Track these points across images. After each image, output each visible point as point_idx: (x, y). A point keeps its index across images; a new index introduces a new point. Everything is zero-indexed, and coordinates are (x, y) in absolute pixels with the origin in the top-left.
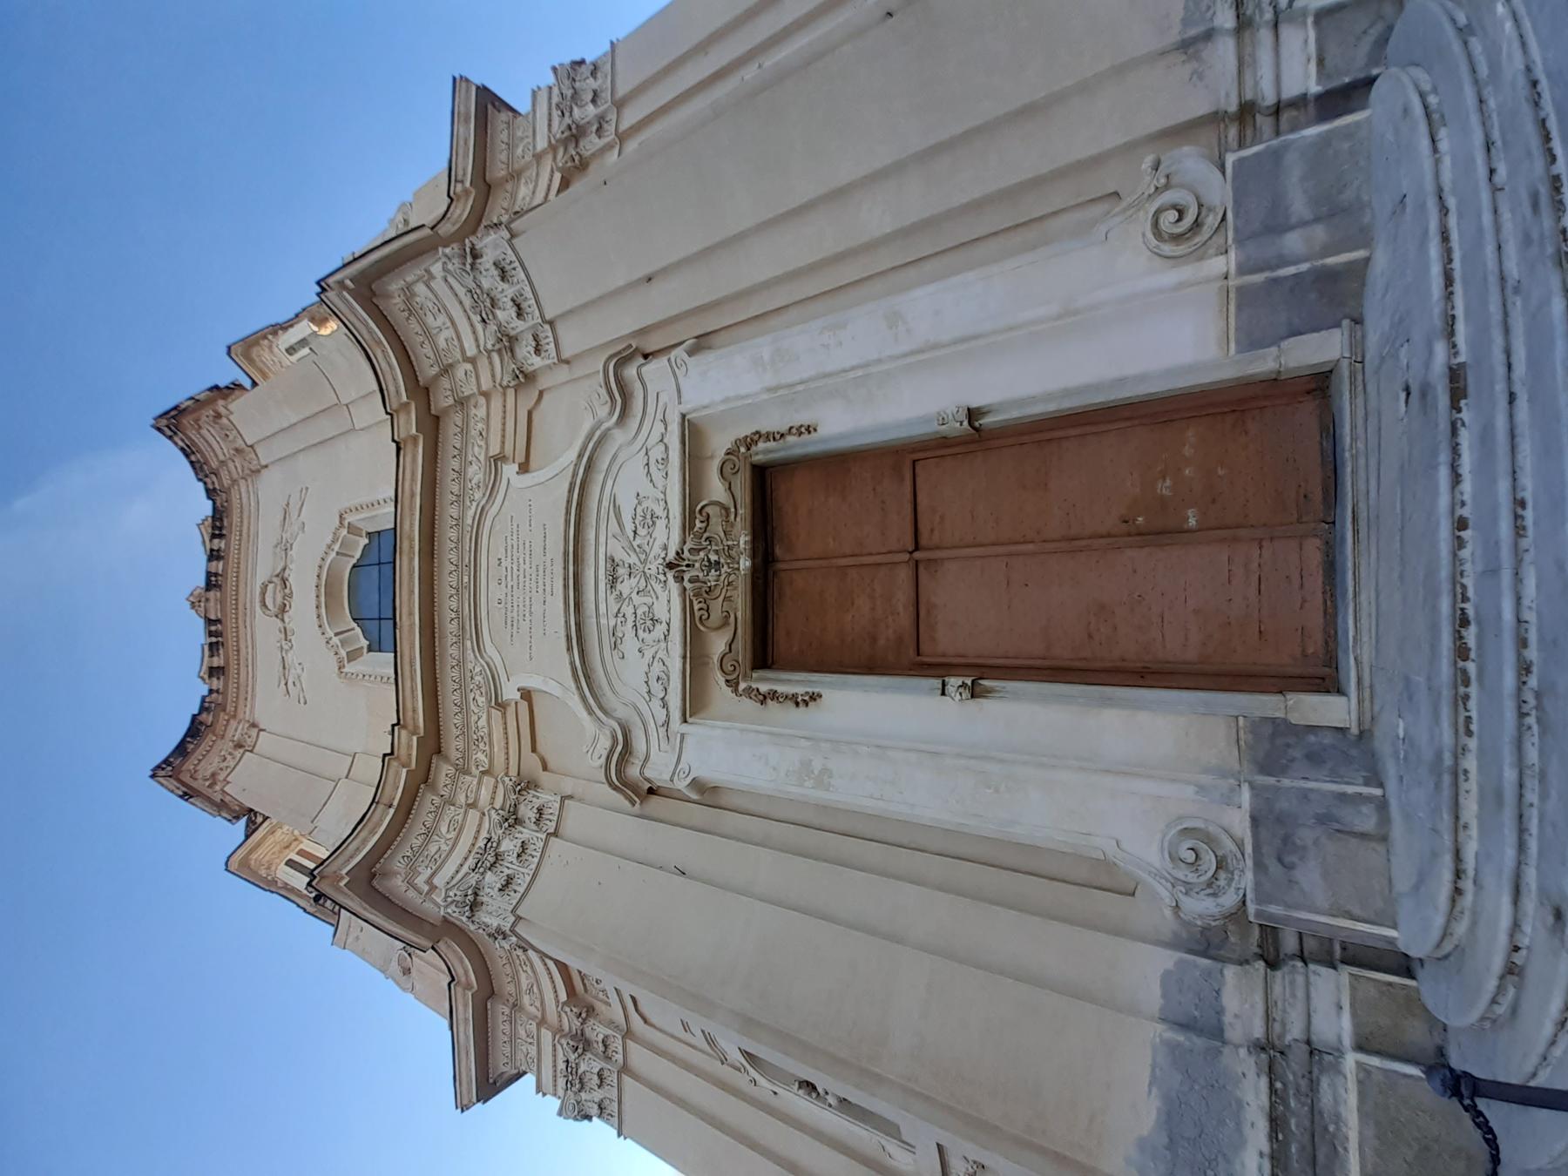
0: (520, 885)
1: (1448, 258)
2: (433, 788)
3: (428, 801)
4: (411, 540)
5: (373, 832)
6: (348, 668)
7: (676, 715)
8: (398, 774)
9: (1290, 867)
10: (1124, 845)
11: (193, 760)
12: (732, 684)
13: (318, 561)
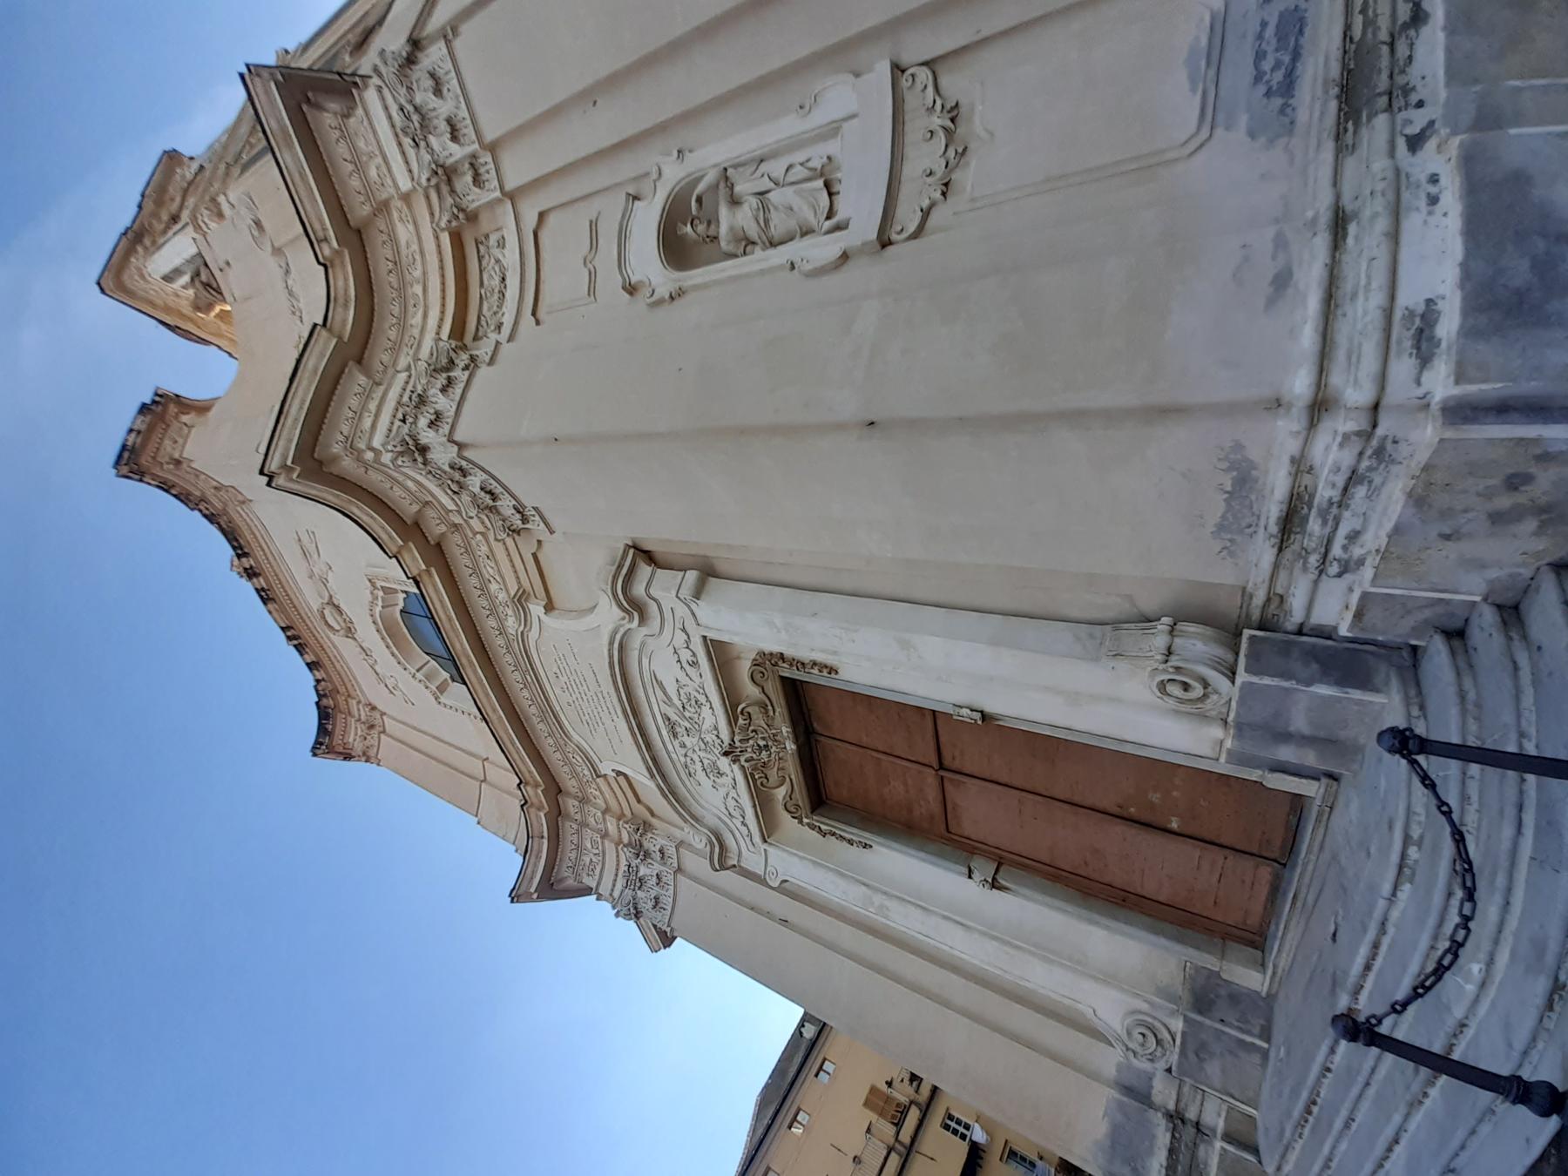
0: (667, 901)
1: (1373, 956)
2: (568, 817)
3: (569, 828)
4: (468, 657)
5: (538, 857)
7: (757, 838)
8: (538, 817)
9: (1201, 1060)
10: (1099, 1013)
11: (338, 731)
13: (373, 628)
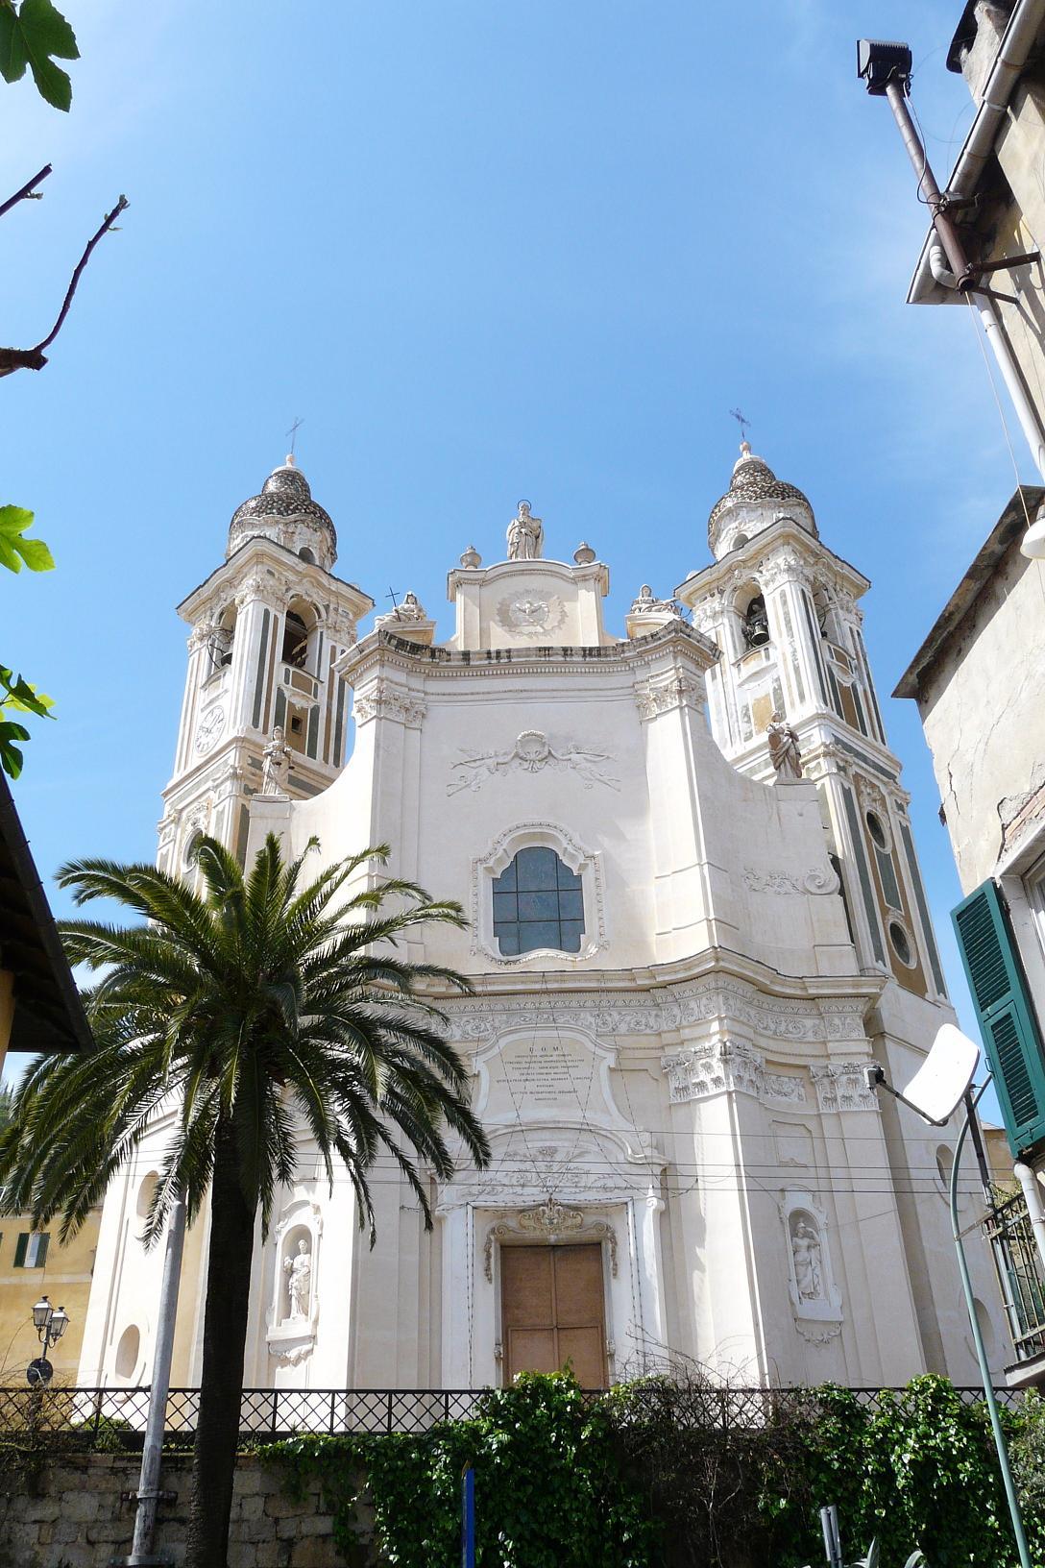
6: (481, 868)
12: (493, 1231)
